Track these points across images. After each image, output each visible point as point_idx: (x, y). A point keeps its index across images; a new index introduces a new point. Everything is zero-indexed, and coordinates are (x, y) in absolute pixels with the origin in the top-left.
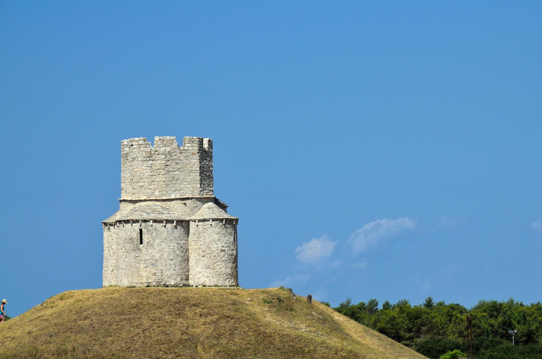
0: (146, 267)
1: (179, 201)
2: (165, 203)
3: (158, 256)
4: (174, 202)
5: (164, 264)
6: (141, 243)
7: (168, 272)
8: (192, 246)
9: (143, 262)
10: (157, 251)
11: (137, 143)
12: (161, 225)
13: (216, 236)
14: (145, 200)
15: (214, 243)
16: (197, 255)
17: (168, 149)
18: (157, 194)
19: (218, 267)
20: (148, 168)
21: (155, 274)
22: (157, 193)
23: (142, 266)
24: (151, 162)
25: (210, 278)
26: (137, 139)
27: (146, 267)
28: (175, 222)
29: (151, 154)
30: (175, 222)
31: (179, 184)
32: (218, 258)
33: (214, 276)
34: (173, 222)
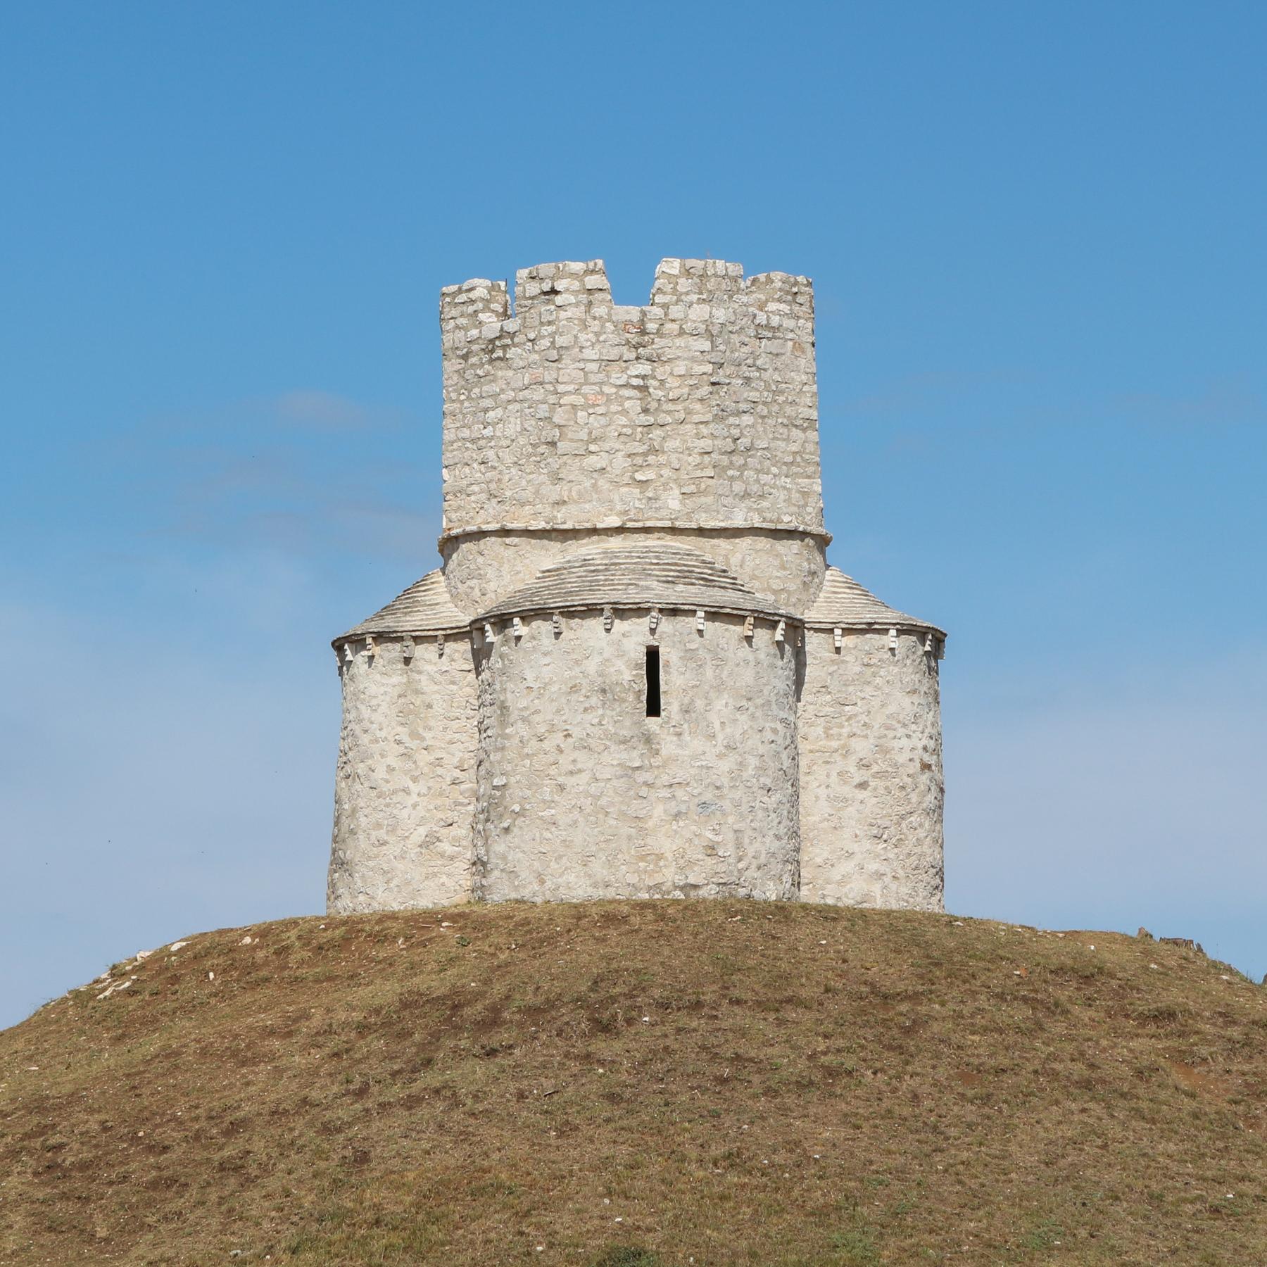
0: (677, 815)
1: (763, 543)
2: (702, 541)
3: (725, 766)
4: (745, 543)
5: (745, 808)
6: (654, 708)
7: (757, 845)
8: (812, 735)
9: (665, 793)
10: (720, 749)
11: (576, 285)
12: (738, 630)
13: (907, 701)
14: (620, 530)
15: (901, 731)
16: (834, 778)
17: (721, 315)
18: (672, 505)
19: (912, 839)
20: (627, 392)
21: (711, 850)
22: (673, 501)
23: (659, 810)
24: (643, 368)
25: (887, 879)
26: (577, 266)
27: (677, 815)
28: (782, 625)
29: (643, 332)
30: (782, 625)
31: (758, 471)
32: (914, 798)
33: (901, 873)
34: (773, 625)
